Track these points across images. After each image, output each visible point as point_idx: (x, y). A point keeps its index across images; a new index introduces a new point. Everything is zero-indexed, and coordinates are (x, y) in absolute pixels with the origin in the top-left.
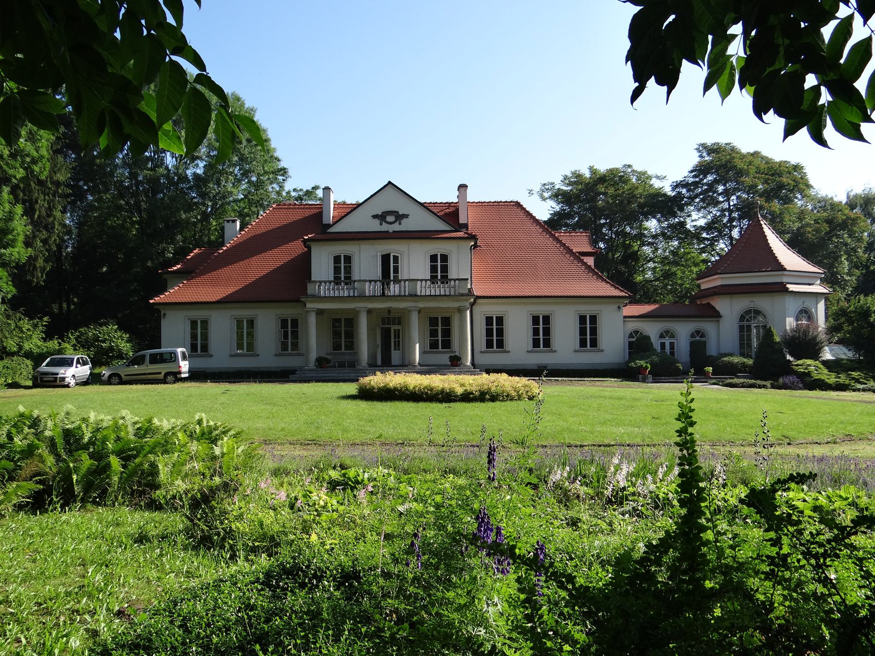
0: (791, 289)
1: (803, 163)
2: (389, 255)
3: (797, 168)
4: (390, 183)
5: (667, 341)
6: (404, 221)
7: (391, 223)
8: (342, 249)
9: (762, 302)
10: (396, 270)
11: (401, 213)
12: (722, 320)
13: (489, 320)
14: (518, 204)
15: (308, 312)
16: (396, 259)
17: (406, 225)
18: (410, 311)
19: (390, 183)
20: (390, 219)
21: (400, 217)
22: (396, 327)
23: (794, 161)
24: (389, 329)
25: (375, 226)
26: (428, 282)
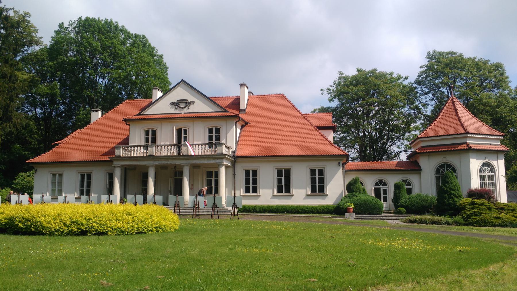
0: (473, 148)
1: (501, 61)
2: (181, 129)
3: (498, 67)
4: (182, 80)
5: (382, 188)
6: (191, 107)
7: (183, 108)
8: (151, 126)
9: (453, 160)
10: (185, 138)
11: (189, 101)
12: (422, 173)
13: (247, 173)
14: (283, 95)
15: (114, 167)
16: (185, 131)
17: (192, 109)
18: (183, 166)
19: (182, 80)
20: (182, 105)
21: (188, 104)
22: (385, 188)
23: (493, 61)
24: (380, 189)
25: (172, 110)
26: (207, 146)
